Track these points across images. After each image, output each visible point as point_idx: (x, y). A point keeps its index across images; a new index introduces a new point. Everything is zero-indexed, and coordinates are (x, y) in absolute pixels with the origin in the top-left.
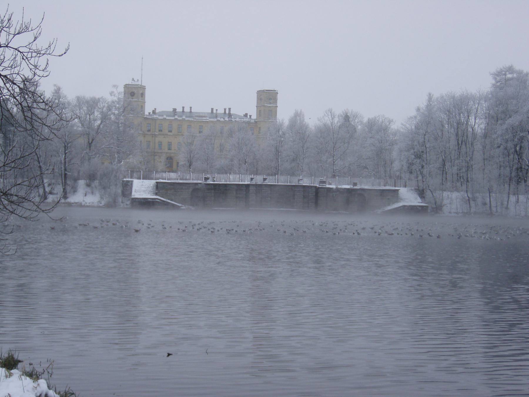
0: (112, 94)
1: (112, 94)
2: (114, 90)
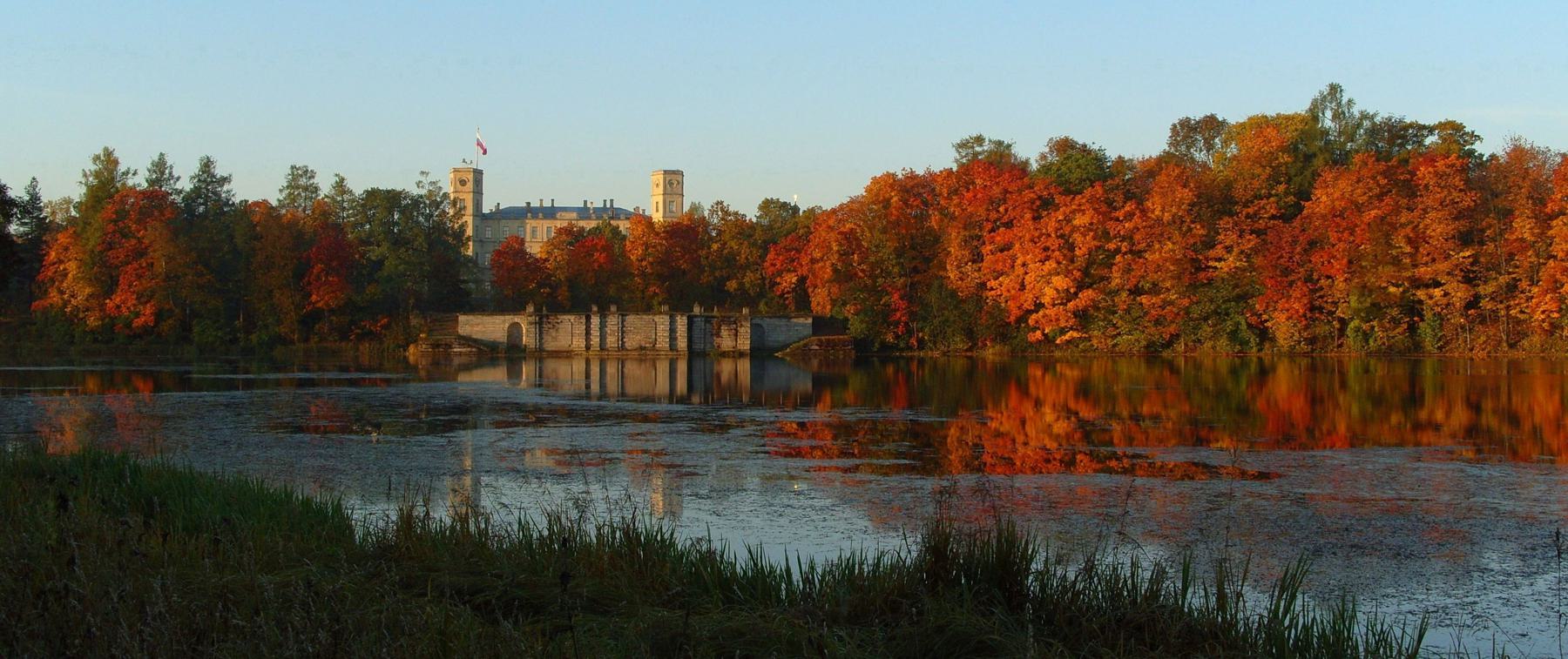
0: (419, 184)
1: (419, 184)
2: (422, 178)
